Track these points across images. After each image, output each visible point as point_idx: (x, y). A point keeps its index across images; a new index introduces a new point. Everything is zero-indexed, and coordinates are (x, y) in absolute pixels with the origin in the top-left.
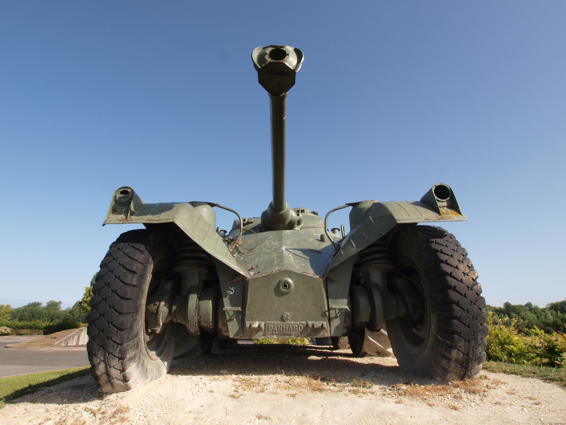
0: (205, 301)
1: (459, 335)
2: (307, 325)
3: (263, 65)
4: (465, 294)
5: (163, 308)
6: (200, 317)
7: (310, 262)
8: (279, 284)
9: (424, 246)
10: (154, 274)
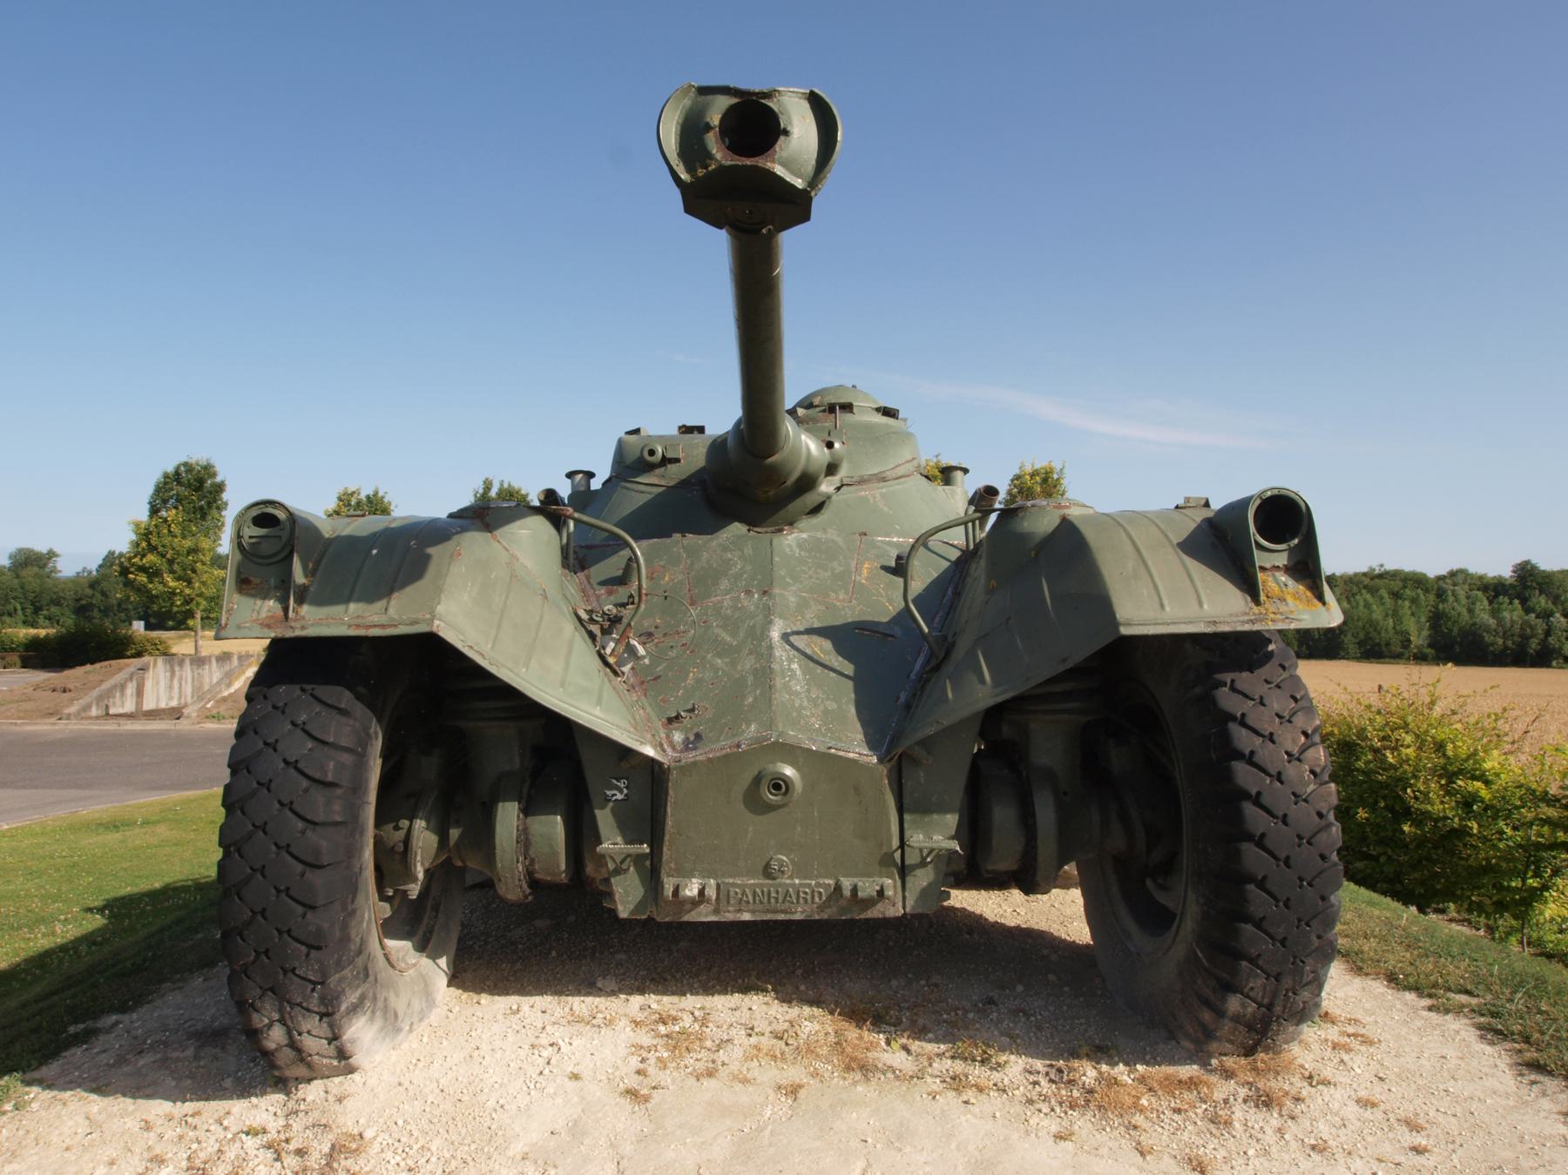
1: (1253, 961)
2: (838, 888)
3: (701, 172)
4: (1288, 858)
5: (424, 838)
6: (532, 861)
7: (857, 691)
8: (758, 780)
9: (1198, 690)
10: (386, 755)
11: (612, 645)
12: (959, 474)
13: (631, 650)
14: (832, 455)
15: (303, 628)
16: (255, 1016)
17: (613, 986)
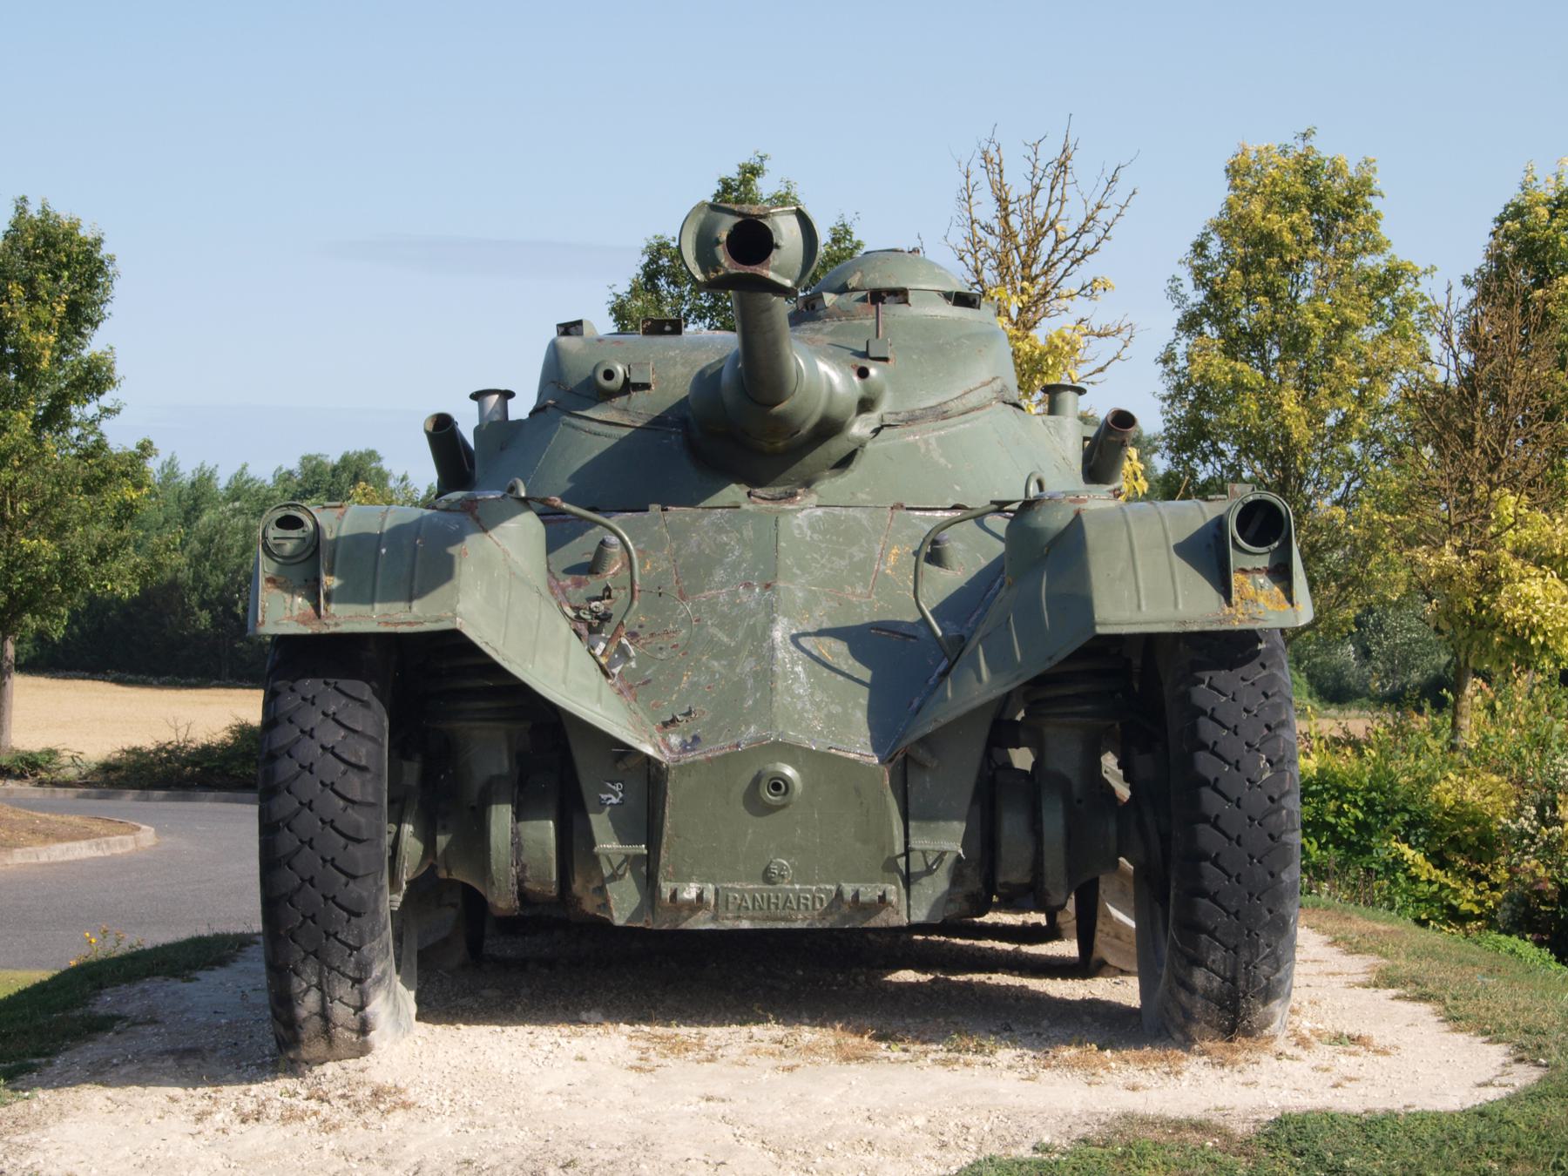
0: (534, 823)
1: (1211, 934)
2: (839, 893)
3: (713, 275)
6: (524, 867)
8: (757, 781)
9: (1182, 688)
11: (602, 645)
12: (1069, 396)
13: (622, 651)
14: (866, 387)
15: (337, 625)
16: (295, 980)
17: (599, 1017)
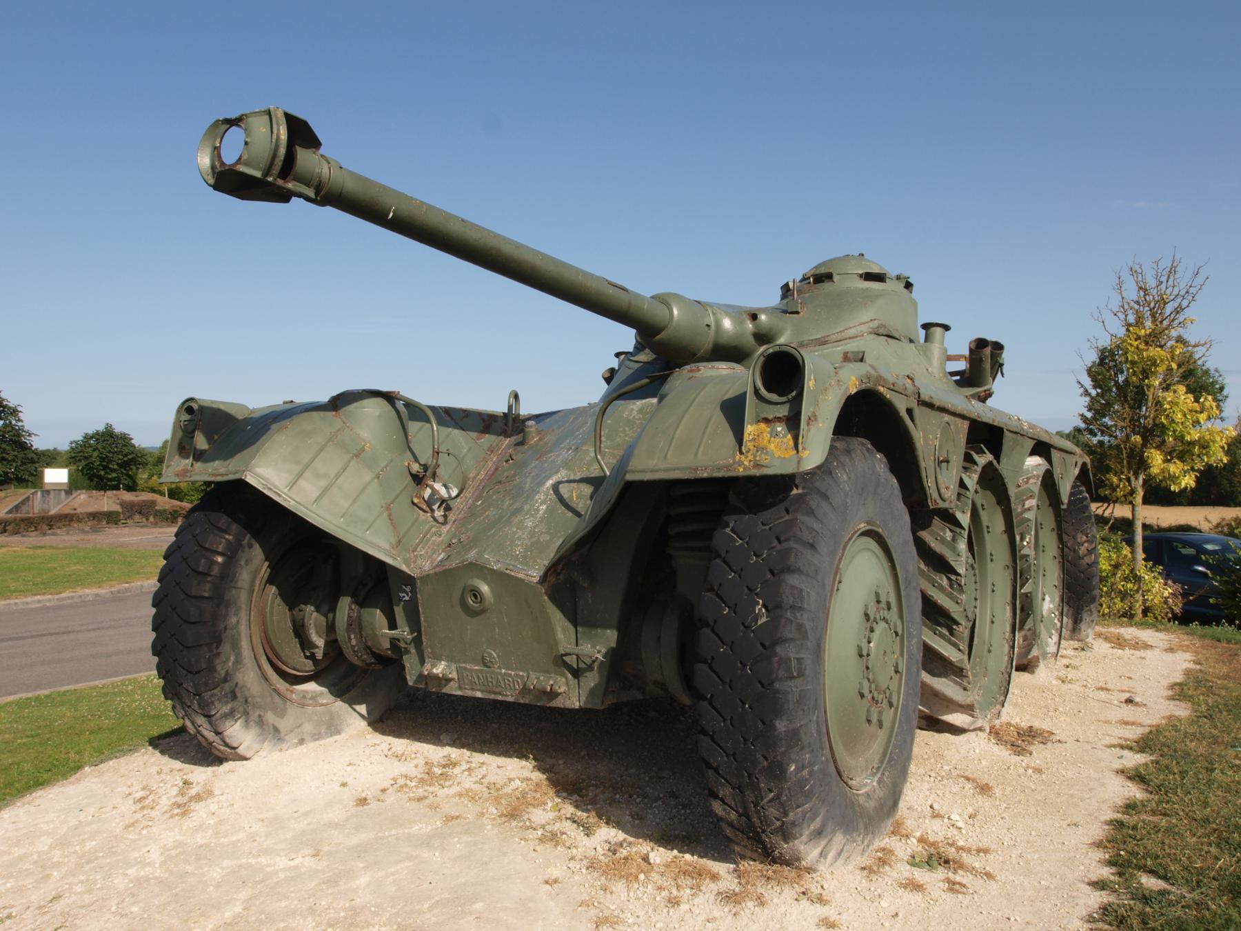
8: (464, 588)
